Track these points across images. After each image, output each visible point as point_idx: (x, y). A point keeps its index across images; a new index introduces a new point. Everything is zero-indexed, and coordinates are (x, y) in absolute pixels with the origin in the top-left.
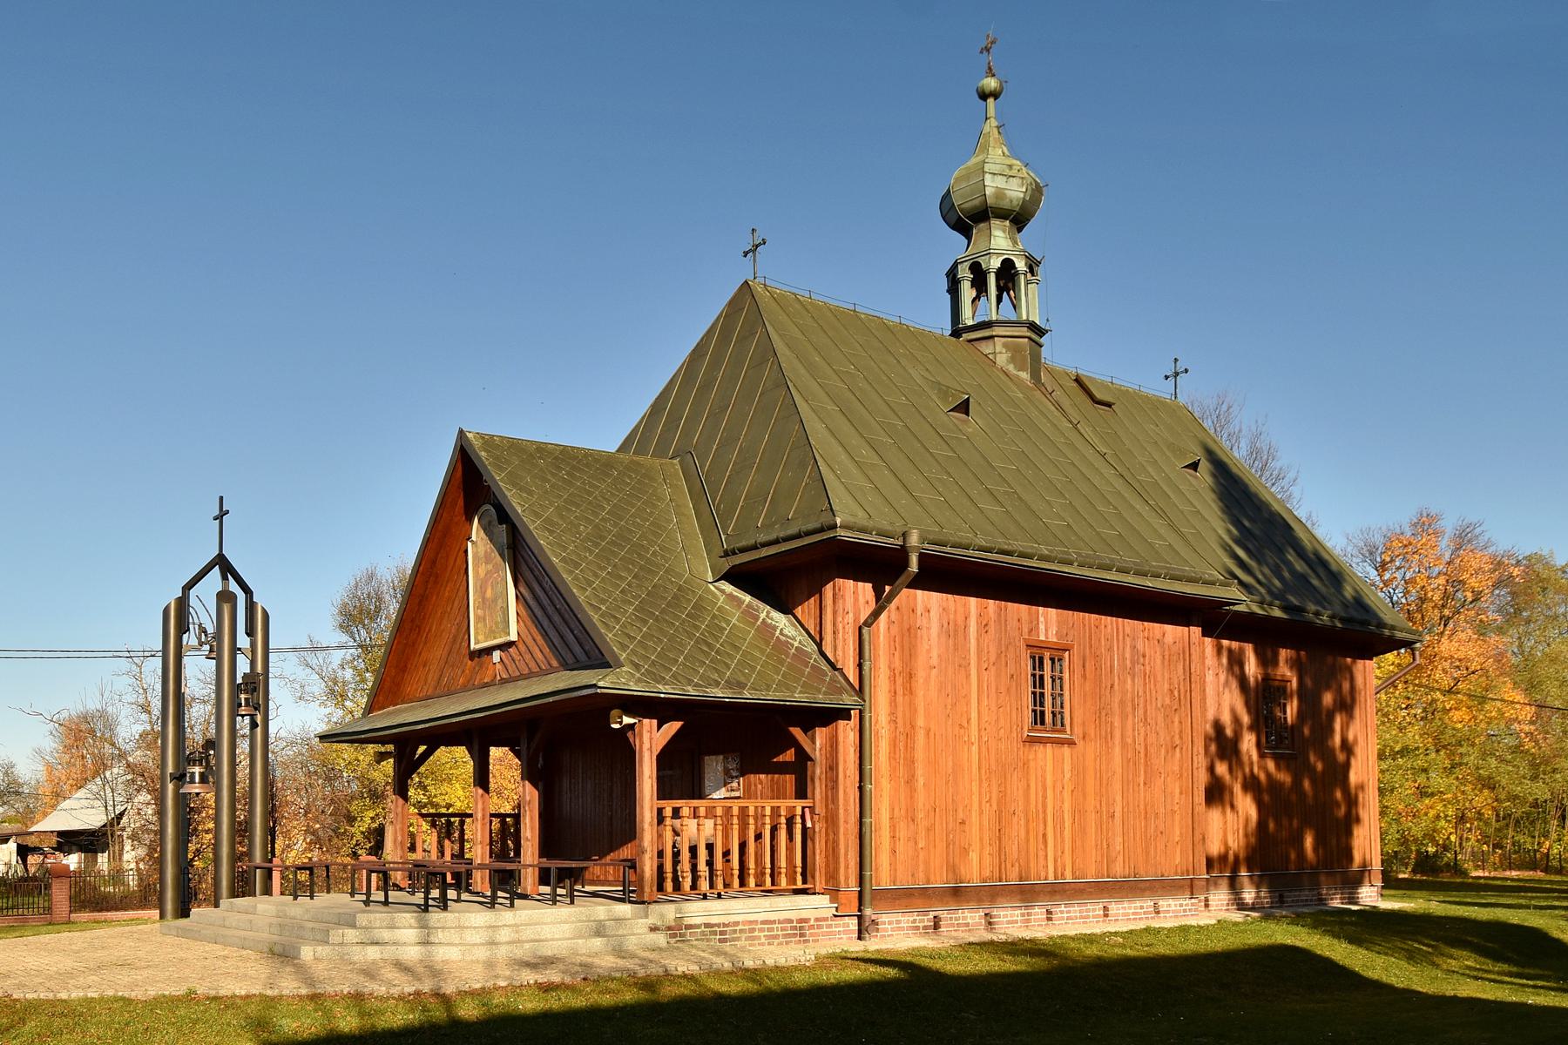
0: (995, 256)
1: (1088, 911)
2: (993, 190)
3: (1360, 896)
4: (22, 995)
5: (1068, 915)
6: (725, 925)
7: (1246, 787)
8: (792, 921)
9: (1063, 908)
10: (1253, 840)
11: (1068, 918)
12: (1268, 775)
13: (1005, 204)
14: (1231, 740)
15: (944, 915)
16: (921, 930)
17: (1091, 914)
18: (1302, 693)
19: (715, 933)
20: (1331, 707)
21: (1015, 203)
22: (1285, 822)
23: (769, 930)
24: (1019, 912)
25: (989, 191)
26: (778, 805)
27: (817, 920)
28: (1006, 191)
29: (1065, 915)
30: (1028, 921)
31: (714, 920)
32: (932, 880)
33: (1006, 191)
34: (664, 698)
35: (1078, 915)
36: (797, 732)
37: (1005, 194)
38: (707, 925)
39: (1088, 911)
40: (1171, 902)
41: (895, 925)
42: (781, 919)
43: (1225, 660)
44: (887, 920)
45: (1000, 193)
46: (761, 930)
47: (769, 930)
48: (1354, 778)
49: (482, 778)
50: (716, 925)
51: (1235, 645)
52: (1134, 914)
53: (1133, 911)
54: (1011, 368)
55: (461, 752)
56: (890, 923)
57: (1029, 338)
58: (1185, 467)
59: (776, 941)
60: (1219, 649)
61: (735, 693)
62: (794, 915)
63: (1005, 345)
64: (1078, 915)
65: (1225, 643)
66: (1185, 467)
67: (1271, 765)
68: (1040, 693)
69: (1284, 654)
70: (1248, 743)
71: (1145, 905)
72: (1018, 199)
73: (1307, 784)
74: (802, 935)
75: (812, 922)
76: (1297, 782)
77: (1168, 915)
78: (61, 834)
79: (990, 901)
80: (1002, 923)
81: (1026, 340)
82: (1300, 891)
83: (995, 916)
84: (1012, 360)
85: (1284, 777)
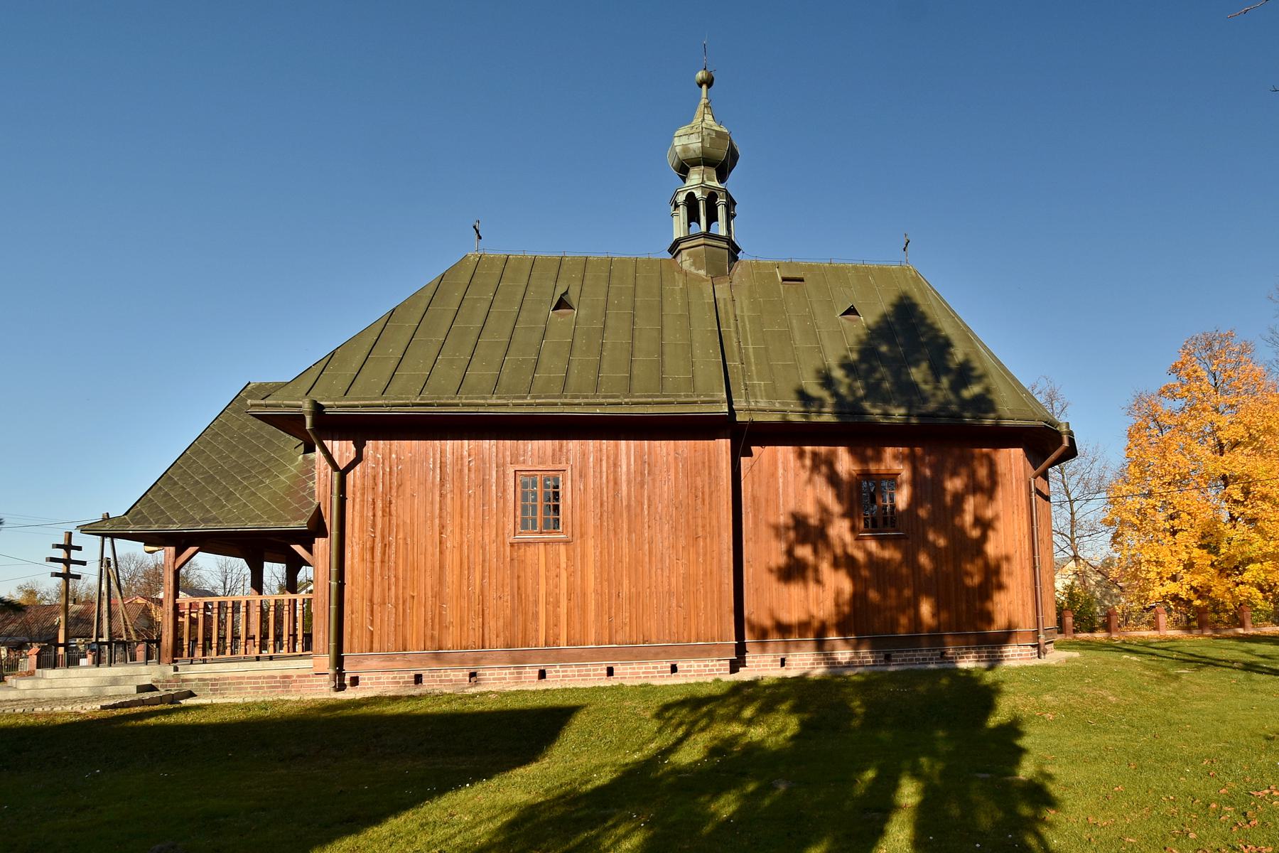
0: (681, 194)
1: (590, 670)
2: (680, 147)
3: (1005, 654)
4: (49, 709)
5: (563, 674)
6: (215, 680)
7: (836, 565)
8: (276, 677)
9: (558, 668)
10: (846, 609)
11: (563, 676)
12: (869, 554)
13: (692, 155)
14: (815, 527)
15: (425, 674)
16: (401, 684)
17: (592, 673)
18: (916, 482)
19: (207, 685)
20: (960, 491)
21: (698, 152)
22: (893, 592)
23: (254, 683)
24: (507, 671)
25: (678, 149)
26: (283, 598)
27: (299, 676)
28: (689, 146)
29: (561, 674)
30: (520, 678)
31: (208, 676)
32: (364, 650)
33: (689, 146)
34: (132, 533)
35: (576, 673)
36: (298, 548)
37: (689, 148)
38: (200, 680)
39: (590, 670)
40: (692, 663)
41: (374, 681)
42: (266, 676)
43: (808, 462)
44: (367, 677)
45: (686, 148)
46: (247, 683)
47: (254, 683)
48: (992, 549)
49: (257, 584)
50: (207, 680)
51: (823, 449)
52: (644, 673)
53: (644, 670)
54: (693, 269)
55: (72, 573)
56: (369, 679)
57: (704, 244)
58: (842, 315)
59: (260, 691)
60: (801, 455)
61: (189, 527)
62: (278, 673)
63: (689, 255)
64: (576, 673)
65: (808, 448)
66: (842, 315)
67: (872, 546)
68: (554, 505)
69: (889, 451)
70: (840, 530)
71: (659, 666)
72: (699, 148)
73: (924, 560)
74: (284, 687)
75: (294, 678)
76: (910, 559)
77: (688, 674)
78: (538, 612)
79: (474, 663)
80: (489, 679)
81: (703, 247)
82: (916, 651)
83: (480, 675)
84: (694, 264)
85: (889, 553)
